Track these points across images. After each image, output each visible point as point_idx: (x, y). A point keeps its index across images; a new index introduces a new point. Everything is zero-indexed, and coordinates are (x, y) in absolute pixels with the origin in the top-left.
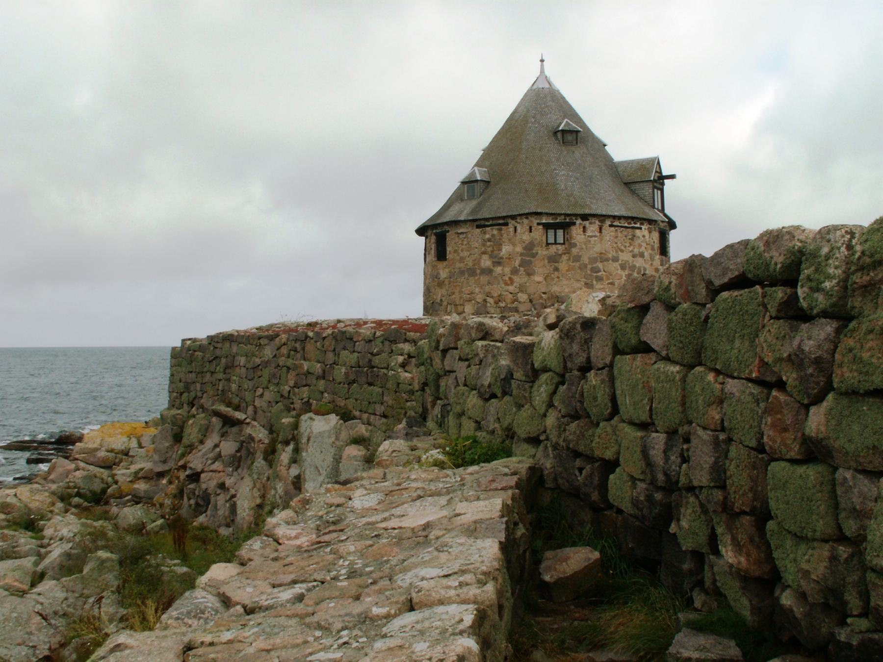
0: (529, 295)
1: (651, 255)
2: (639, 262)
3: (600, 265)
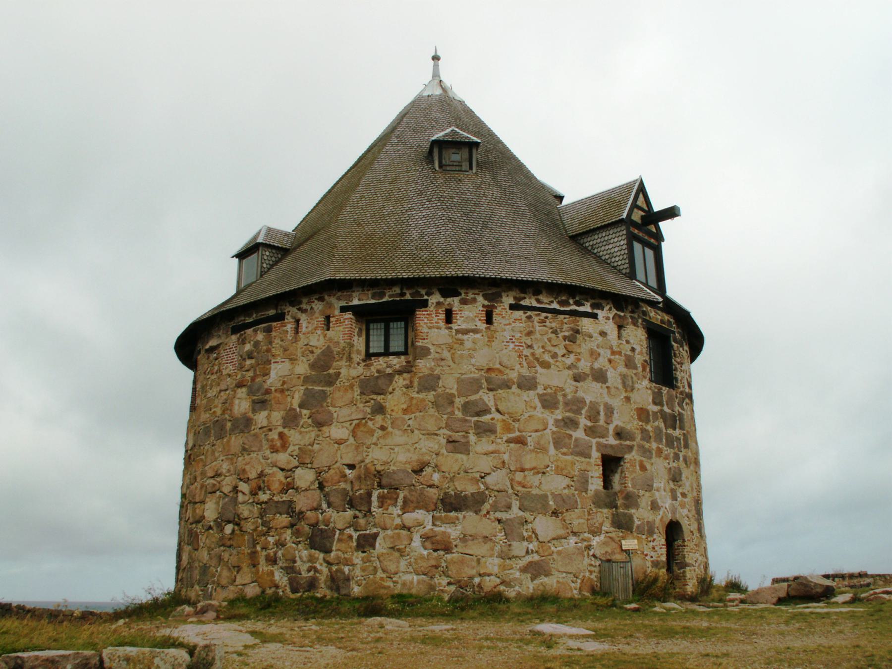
1: (624, 377)
2: (591, 392)
3: (488, 398)
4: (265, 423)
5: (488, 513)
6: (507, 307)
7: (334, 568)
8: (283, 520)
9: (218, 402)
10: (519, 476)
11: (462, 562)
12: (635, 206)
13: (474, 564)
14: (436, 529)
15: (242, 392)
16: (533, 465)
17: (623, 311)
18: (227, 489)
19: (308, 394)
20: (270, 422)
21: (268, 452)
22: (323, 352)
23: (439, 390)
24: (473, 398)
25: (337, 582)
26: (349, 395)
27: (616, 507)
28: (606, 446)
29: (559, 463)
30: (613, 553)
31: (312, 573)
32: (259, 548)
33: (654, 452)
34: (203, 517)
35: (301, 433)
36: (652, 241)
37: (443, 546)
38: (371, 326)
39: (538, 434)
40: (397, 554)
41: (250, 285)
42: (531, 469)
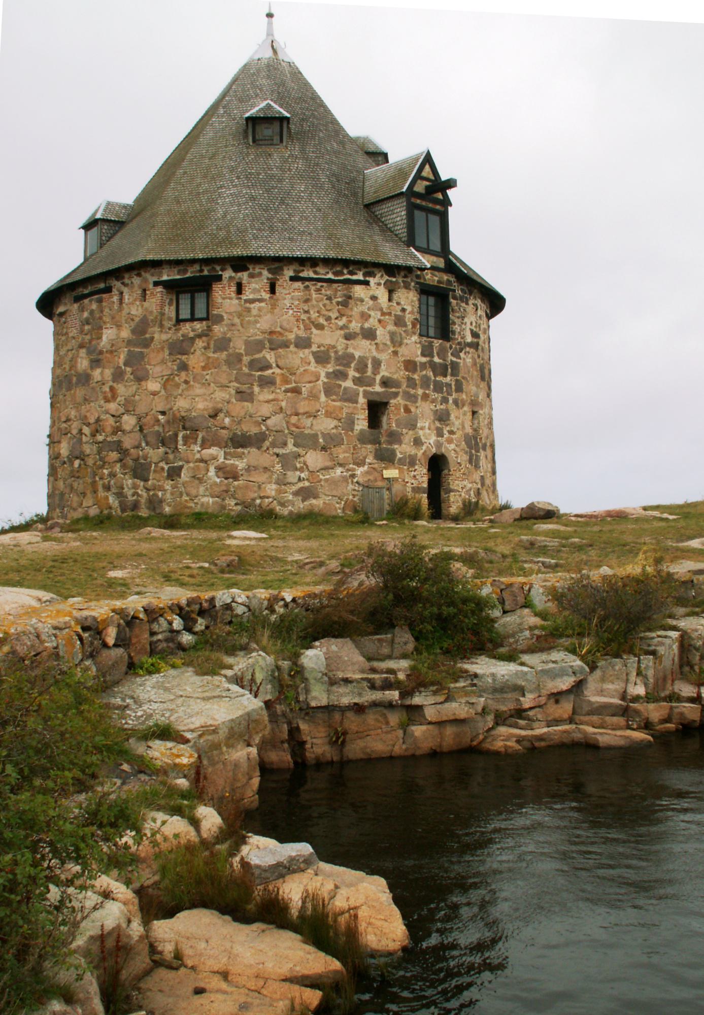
0: (139, 419)
1: (392, 335)
2: (361, 348)
4: (99, 379)
5: (268, 449)
6: (288, 278)
7: (151, 493)
8: (114, 456)
9: (67, 360)
10: (294, 419)
11: (247, 487)
12: (418, 176)
13: (256, 489)
14: (227, 462)
15: (83, 352)
16: (307, 409)
17: (395, 277)
18: (75, 432)
19: (130, 354)
20: (103, 378)
21: (102, 402)
22: (141, 319)
23: (230, 351)
24: (257, 356)
25: (154, 503)
26: (161, 356)
27: (380, 443)
28: (372, 393)
29: (329, 409)
30: (376, 480)
31: (135, 498)
32: (97, 479)
33: (420, 398)
34: (59, 454)
35: (125, 386)
36: (438, 207)
37: (232, 475)
38: (180, 296)
39: (312, 385)
40: (197, 482)
41: (92, 255)
42: (304, 414)
